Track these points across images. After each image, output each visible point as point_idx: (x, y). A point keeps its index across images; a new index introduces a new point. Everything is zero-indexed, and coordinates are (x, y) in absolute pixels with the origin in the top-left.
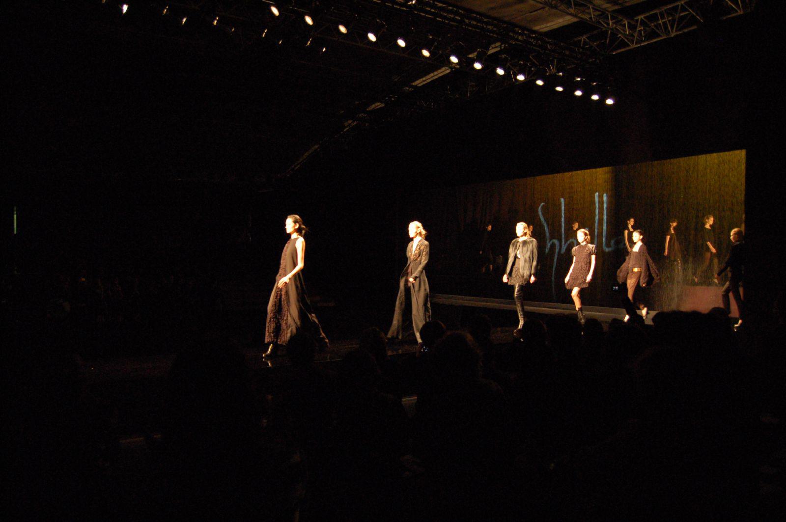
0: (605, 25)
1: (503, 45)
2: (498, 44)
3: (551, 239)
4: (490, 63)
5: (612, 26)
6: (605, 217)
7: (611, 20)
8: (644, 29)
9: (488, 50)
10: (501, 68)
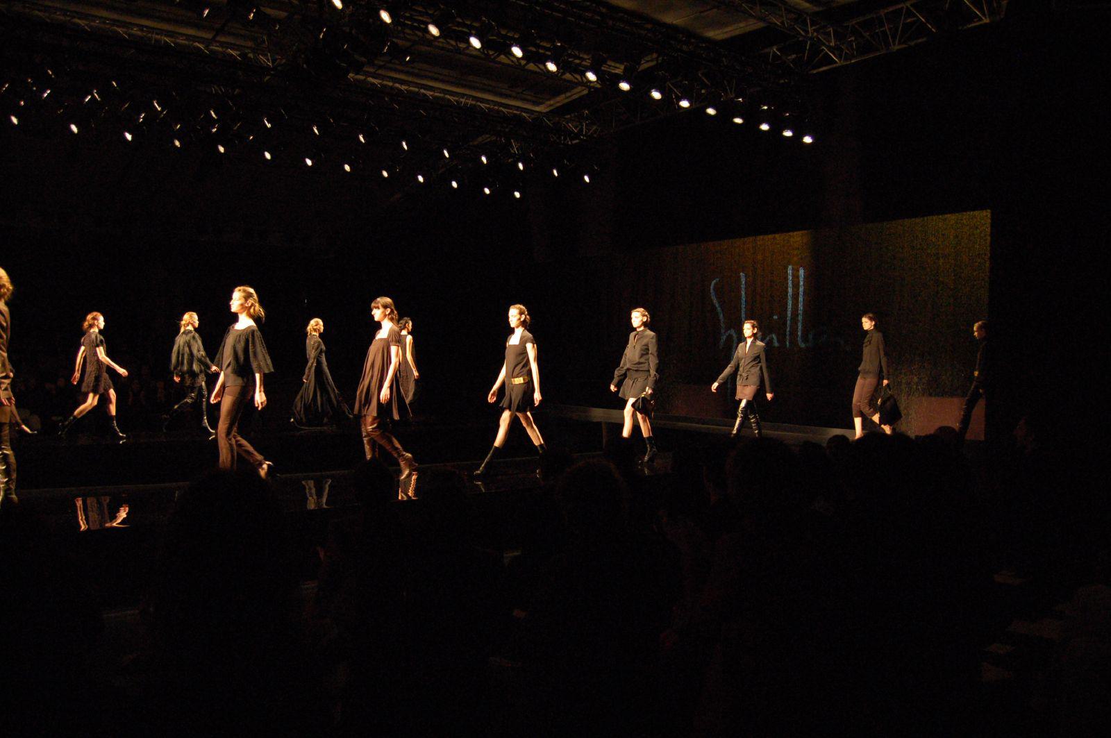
0: (803, 33)
1: (661, 58)
2: (655, 56)
3: (728, 328)
4: (642, 84)
5: (812, 34)
6: (801, 306)
7: (811, 26)
8: (856, 39)
9: (639, 64)
10: (656, 91)
